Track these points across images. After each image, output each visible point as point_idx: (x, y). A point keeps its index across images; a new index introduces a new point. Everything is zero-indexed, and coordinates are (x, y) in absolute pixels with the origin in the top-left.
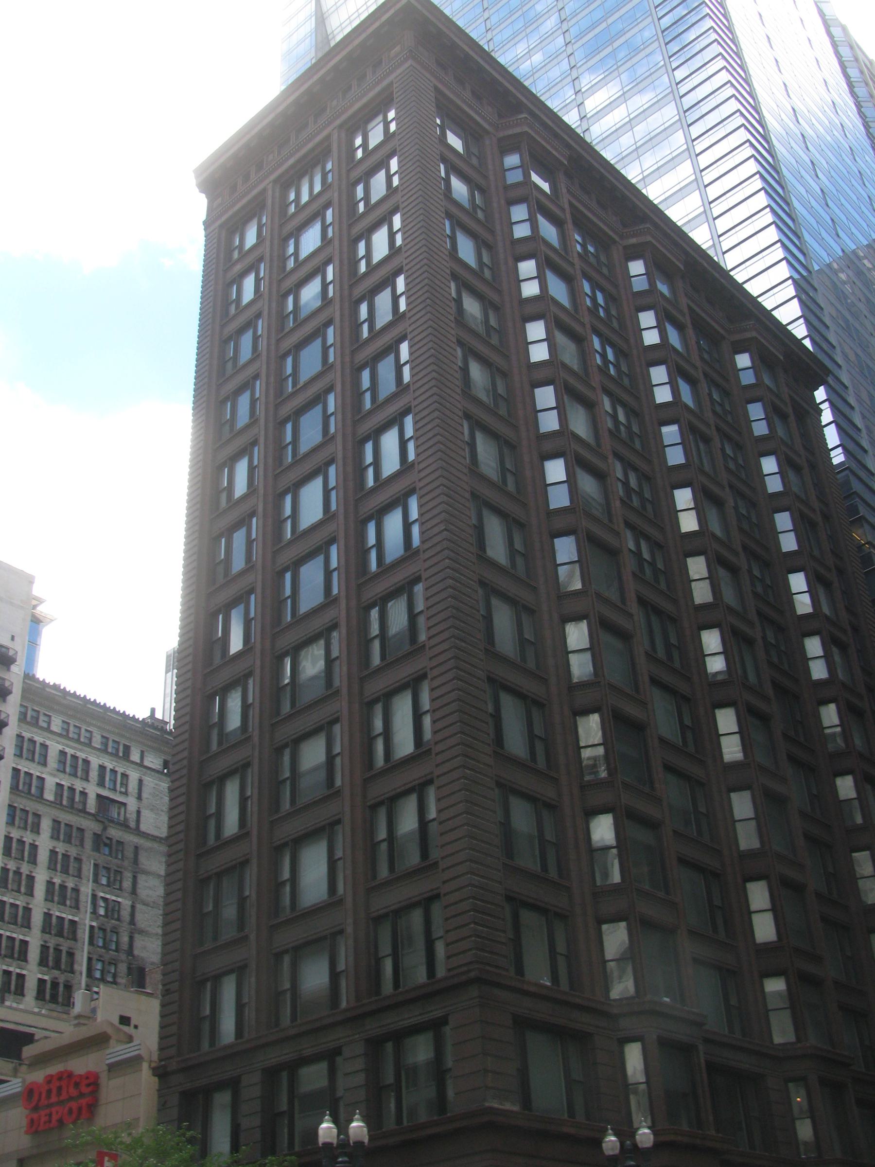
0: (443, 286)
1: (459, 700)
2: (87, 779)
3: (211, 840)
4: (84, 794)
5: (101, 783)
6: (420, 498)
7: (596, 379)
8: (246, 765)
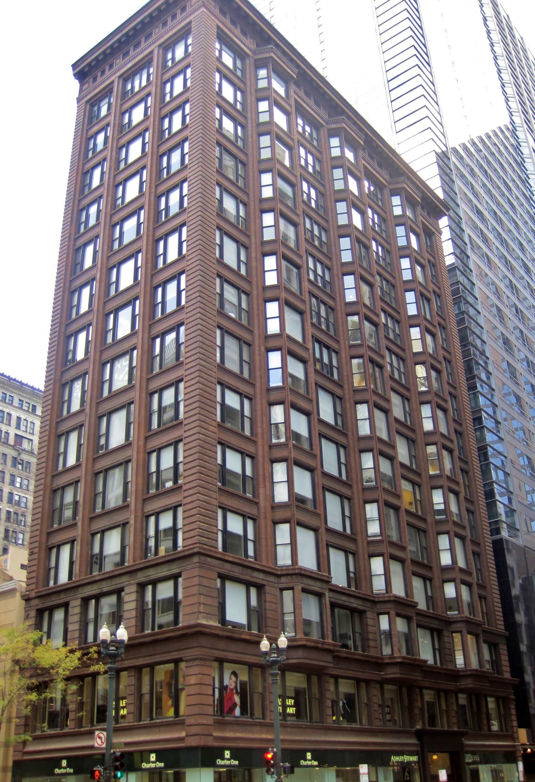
0: (210, 150)
1: (199, 395)
2: (9, 425)
3: (60, 468)
4: (7, 433)
5: (18, 427)
6: (187, 276)
7: (301, 207)
8: (81, 426)
